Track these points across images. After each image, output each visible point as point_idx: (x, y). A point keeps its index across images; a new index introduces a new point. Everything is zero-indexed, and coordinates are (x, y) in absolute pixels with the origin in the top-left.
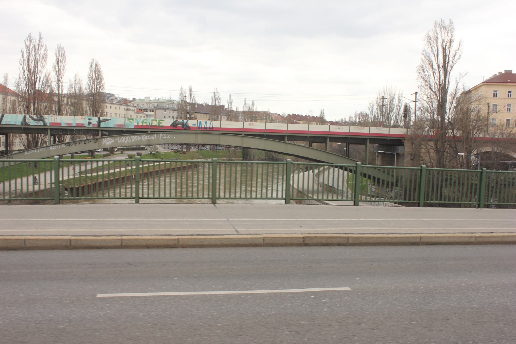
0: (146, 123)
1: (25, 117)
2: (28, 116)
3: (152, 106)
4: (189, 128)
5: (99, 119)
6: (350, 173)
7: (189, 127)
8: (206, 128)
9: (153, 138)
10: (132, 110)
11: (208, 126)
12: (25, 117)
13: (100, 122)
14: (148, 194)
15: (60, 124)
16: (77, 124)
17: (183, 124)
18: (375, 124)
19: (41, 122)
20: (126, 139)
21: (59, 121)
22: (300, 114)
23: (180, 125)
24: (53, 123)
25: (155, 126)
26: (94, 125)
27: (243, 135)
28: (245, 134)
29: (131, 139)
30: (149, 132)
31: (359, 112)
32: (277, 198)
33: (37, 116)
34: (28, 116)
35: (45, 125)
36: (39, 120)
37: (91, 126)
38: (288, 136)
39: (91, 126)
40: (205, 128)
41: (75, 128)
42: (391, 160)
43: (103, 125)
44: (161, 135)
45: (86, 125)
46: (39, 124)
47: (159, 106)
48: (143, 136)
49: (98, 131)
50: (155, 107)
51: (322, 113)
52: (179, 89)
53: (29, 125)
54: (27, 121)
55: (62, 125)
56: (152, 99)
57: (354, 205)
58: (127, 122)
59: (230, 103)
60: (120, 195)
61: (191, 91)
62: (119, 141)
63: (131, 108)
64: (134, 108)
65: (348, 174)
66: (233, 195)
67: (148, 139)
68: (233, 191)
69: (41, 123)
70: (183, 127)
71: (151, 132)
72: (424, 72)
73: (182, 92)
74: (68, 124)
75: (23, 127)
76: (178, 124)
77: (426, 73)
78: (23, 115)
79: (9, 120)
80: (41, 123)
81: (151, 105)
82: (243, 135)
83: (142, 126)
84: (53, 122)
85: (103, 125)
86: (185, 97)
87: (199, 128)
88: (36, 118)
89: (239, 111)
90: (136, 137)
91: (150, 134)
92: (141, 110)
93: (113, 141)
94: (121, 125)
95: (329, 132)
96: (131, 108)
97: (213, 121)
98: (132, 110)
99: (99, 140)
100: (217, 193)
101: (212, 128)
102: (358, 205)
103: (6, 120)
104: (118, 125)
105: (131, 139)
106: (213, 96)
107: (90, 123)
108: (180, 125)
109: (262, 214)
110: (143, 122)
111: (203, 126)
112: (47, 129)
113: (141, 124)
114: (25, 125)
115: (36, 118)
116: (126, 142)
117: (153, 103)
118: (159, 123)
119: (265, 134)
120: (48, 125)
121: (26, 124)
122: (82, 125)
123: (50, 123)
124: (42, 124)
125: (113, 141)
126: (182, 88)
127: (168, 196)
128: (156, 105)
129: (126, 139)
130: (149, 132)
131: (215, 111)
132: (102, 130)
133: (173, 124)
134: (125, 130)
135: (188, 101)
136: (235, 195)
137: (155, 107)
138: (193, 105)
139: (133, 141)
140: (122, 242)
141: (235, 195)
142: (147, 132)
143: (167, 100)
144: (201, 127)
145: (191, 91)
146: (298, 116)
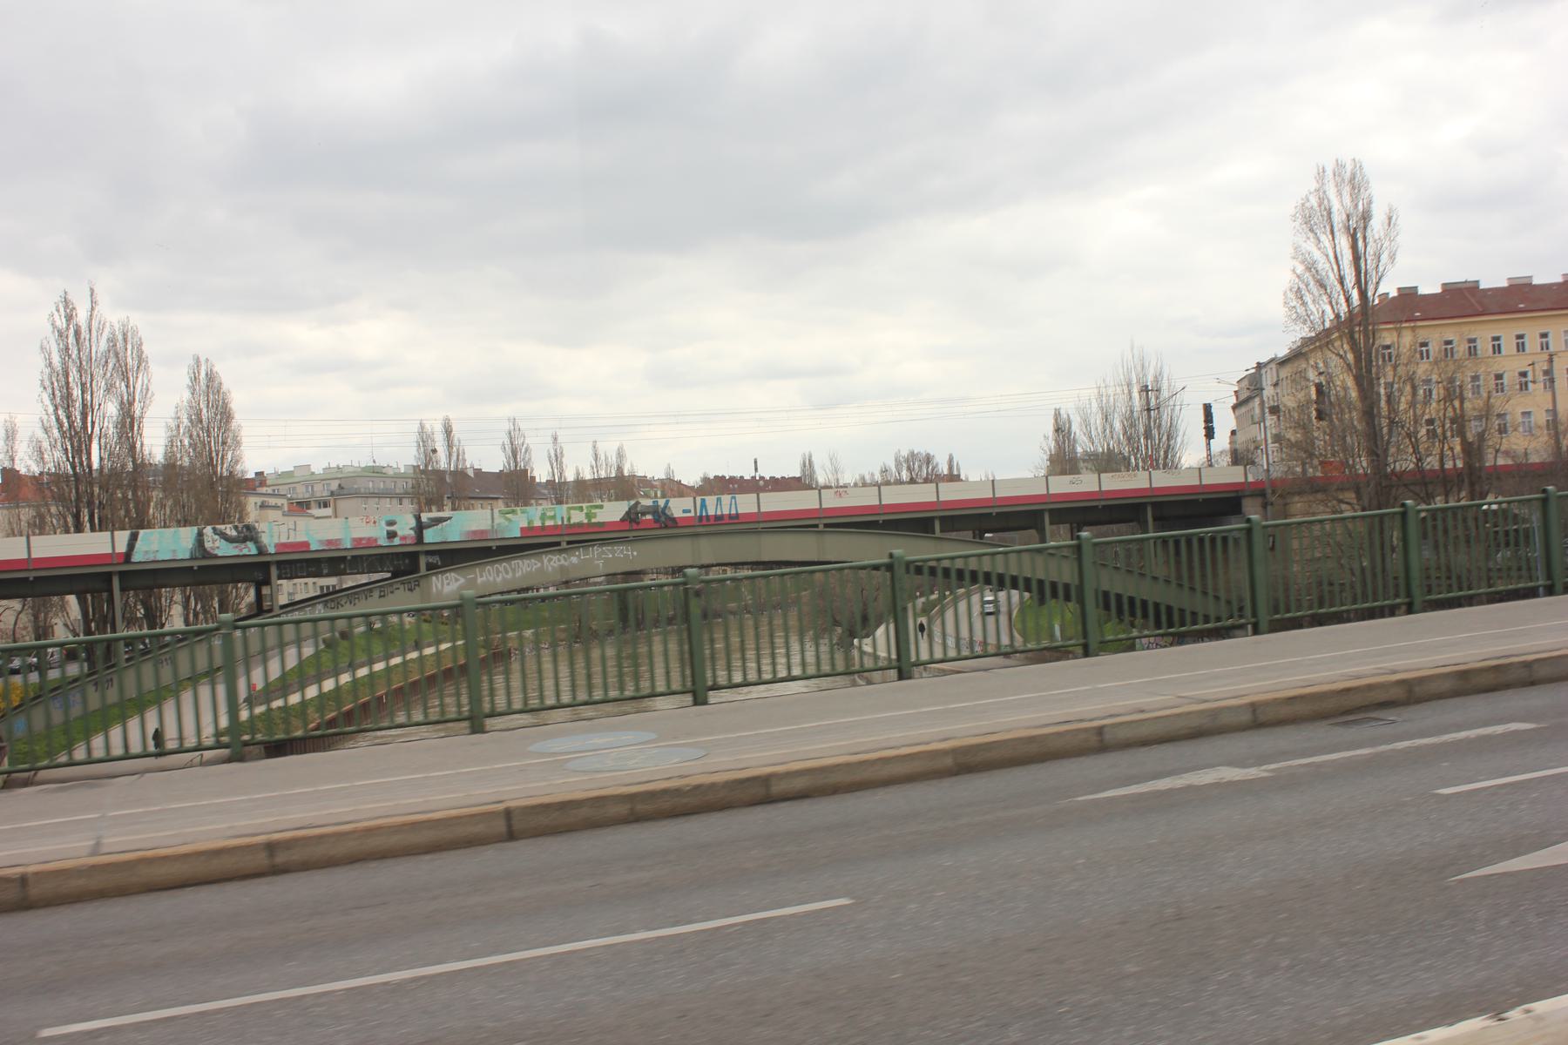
0: (553, 517)
1: (200, 534)
2: (208, 530)
3: (321, 492)
4: (672, 522)
5: (418, 518)
6: (1027, 595)
7: (674, 520)
8: (721, 517)
9: (574, 560)
10: (276, 507)
11: (726, 512)
12: (200, 534)
13: (420, 528)
14: (759, 671)
15: (306, 544)
16: (354, 540)
17: (654, 510)
18: (1107, 462)
19: (250, 545)
20: (498, 572)
21: (300, 538)
22: (737, 474)
23: (649, 517)
24: (284, 545)
25: (580, 525)
26: (403, 538)
27: (821, 528)
28: (826, 525)
29: (514, 570)
30: (564, 545)
31: (905, 453)
32: (790, 678)
33: (236, 528)
34: (208, 530)
35: (262, 551)
36: (245, 540)
37: (397, 541)
38: (942, 519)
39: (397, 541)
40: (717, 518)
41: (349, 554)
42: (1127, 551)
43: (430, 536)
44: (596, 551)
45: (383, 542)
46: (245, 552)
47: (343, 489)
48: (545, 559)
49: (414, 557)
50: (332, 494)
51: (808, 465)
52: (416, 428)
53: (216, 557)
54: (208, 545)
55: (313, 547)
56: (317, 468)
57: (696, 703)
58: (499, 520)
59: (557, 459)
60: (804, 670)
61: (448, 432)
62: (479, 580)
63: (272, 501)
64: (279, 502)
65: (1021, 597)
66: (645, 685)
67: (562, 566)
68: (766, 661)
69: (250, 549)
70: (656, 521)
71: (569, 543)
72: (1304, 304)
73: (424, 438)
74: (329, 542)
75: (196, 564)
76: (644, 514)
77: (1311, 306)
78: (195, 529)
79: (155, 547)
80: (250, 549)
81: (318, 487)
82: (821, 528)
83: (543, 528)
84: (284, 540)
85: (430, 536)
86: (434, 451)
87: (701, 517)
88: (234, 533)
89: (565, 483)
90: (526, 562)
91: (565, 550)
92: (302, 506)
93: (462, 580)
94: (482, 532)
95: (1048, 495)
96: (272, 501)
97: (109, 551)
98: (276, 507)
99: (422, 582)
100: (709, 674)
101: (737, 515)
102: (705, 703)
103: (146, 548)
104: (474, 532)
105: (514, 570)
106: (507, 441)
107: (392, 535)
108: (649, 517)
109: (785, 716)
110: (543, 517)
111: (711, 512)
112: (267, 565)
113: (537, 523)
114: (204, 558)
115: (234, 533)
116: (499, 579)
117: (323, 480)
118: (588, 516)
119: (881, 518)
120: (272, 550)
121: (206, 554)
122: (371, 543)
123: (277, 545)
124: (254, 551)
125: (462, 580)
126: (422, 426)
127: (796, 671)
128: (334, 486)
129: (498, 572)
130: (564, 545)
131: (515, 485)
132: (428, 553)
133: (628, 513)
134: (493, 544)
135: (443, 465)
136: (745, 675)
137: (332, 494)
138: (460, 474)
139: (518, 574)
140: (1254, 711)
141: (745, 675)
142: (558, 544)
143: (366, 469)
144: (708, 517)
145: (448, 432)
146: (732, 479)
